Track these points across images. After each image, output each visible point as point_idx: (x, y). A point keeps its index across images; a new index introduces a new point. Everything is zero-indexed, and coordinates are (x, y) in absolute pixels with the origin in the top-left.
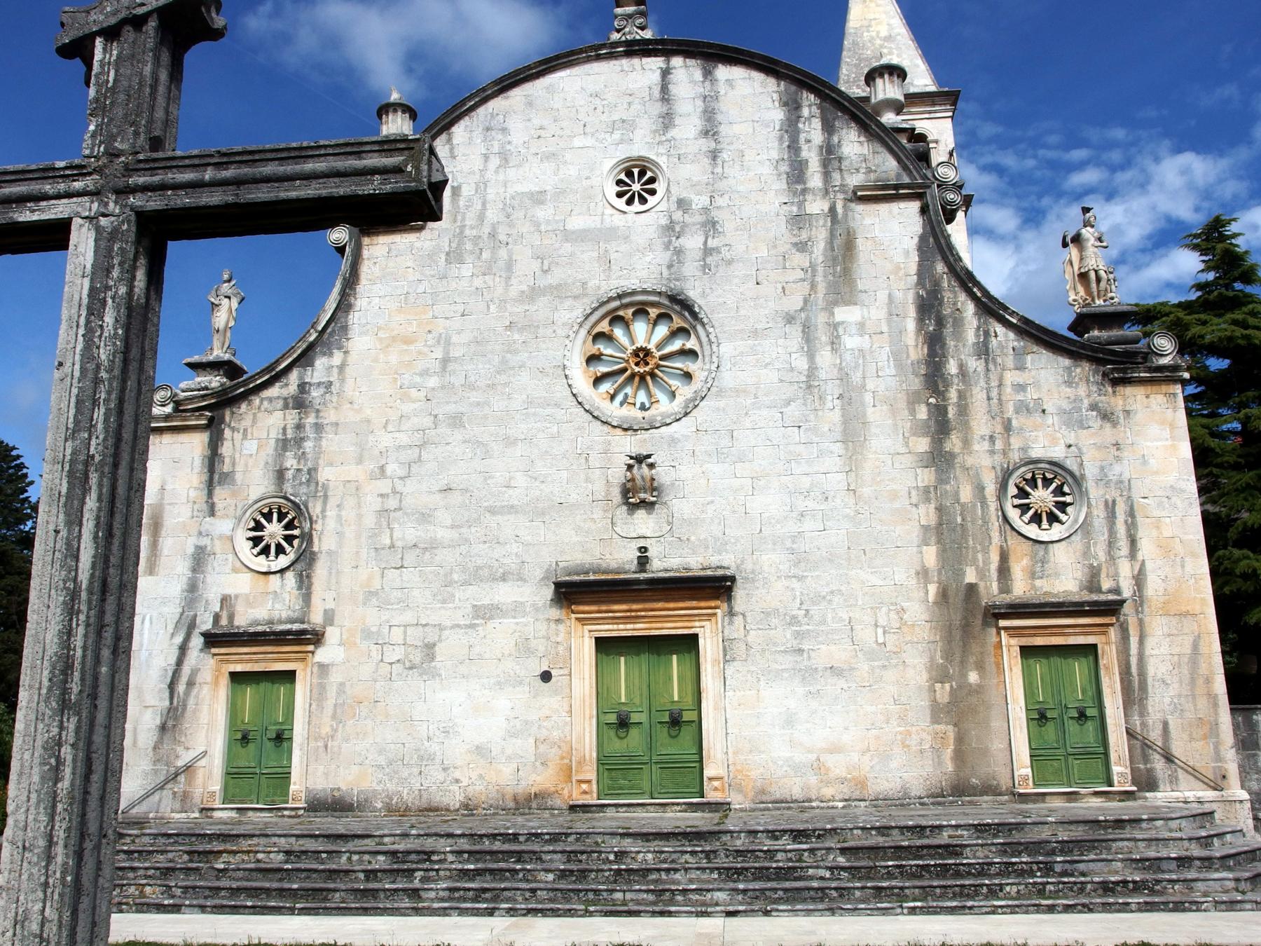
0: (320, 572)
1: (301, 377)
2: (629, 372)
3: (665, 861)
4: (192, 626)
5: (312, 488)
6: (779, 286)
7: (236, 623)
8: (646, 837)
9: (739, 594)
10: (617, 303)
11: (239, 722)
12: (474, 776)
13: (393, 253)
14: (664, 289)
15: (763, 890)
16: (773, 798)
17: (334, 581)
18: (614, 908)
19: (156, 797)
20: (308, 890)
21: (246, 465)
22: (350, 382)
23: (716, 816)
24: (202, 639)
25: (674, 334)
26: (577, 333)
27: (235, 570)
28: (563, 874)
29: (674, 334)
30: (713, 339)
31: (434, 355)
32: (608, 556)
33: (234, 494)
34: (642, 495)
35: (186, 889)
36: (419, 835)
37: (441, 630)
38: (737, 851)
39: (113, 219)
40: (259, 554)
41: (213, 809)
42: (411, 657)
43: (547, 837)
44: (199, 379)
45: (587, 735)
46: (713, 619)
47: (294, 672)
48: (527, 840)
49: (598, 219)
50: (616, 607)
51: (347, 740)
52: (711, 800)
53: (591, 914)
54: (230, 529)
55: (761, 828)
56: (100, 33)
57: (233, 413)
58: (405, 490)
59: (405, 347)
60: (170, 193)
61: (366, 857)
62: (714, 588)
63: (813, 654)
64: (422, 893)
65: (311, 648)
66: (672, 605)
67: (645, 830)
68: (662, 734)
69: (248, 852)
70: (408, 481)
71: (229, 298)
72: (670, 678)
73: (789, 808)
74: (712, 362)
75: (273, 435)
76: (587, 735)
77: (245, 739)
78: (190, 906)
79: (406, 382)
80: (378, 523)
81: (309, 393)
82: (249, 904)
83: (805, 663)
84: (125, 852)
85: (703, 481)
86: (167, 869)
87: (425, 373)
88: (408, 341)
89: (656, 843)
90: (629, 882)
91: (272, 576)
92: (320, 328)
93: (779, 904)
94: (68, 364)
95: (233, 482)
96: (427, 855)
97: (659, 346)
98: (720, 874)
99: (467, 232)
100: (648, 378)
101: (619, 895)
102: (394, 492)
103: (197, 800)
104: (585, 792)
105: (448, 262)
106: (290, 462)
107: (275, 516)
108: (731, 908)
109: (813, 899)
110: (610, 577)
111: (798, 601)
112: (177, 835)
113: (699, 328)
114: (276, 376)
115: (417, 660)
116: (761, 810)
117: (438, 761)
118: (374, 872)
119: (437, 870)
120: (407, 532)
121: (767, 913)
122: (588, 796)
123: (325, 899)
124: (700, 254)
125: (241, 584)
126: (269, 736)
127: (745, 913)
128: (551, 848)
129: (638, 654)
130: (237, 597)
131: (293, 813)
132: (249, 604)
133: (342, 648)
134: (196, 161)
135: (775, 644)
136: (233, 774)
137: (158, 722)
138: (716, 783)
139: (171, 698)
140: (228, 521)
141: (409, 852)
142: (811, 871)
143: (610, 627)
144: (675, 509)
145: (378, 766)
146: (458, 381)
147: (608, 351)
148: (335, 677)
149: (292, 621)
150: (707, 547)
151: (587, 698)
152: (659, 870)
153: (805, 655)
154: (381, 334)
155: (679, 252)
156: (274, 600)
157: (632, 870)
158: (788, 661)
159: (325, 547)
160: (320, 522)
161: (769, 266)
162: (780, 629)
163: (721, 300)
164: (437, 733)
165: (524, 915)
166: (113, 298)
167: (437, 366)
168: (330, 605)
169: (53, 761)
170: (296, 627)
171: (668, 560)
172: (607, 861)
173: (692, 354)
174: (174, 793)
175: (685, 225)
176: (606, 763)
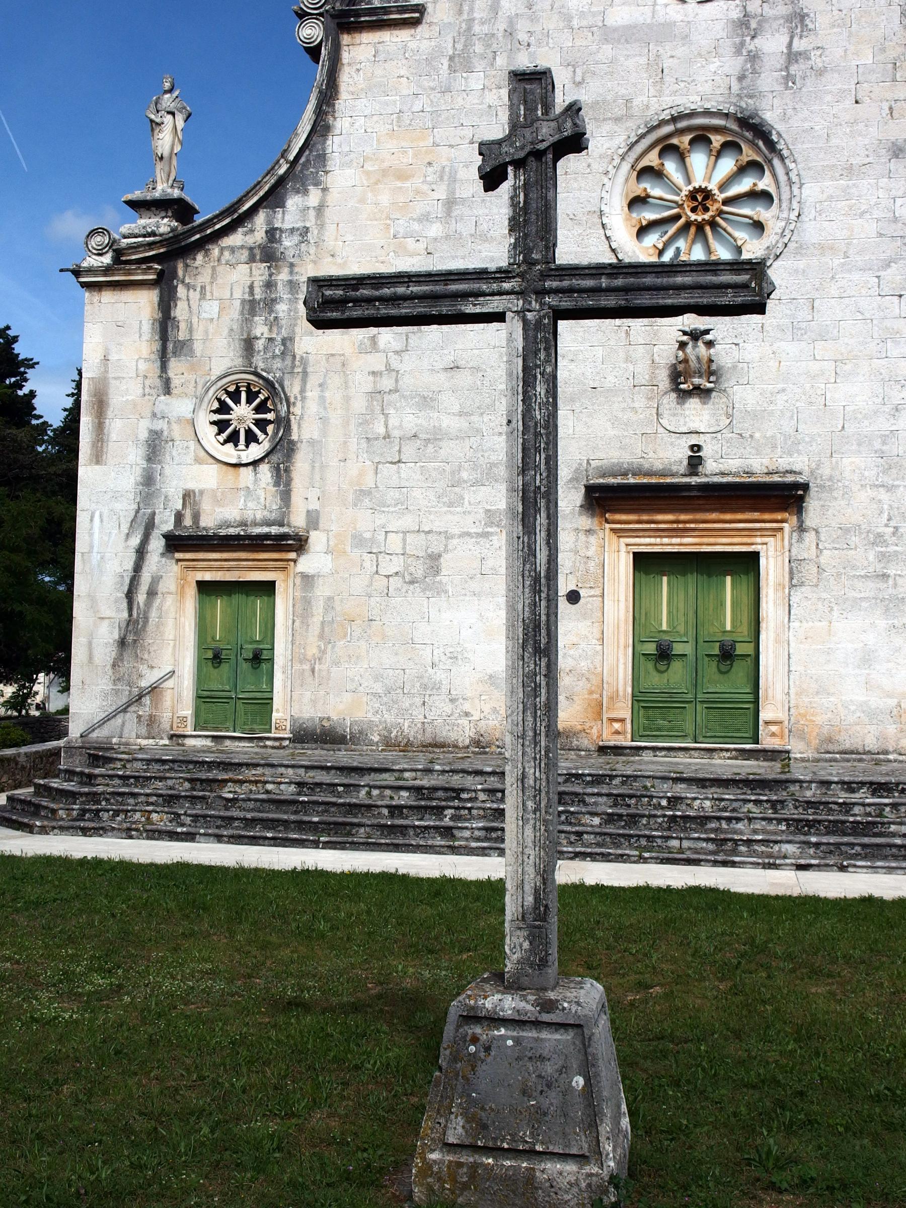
0: (301, 465)
1: (269, 222)
2: (682, 221)
3: (725, 809)
4: (150, 526)
5: (288, 361)
6: (886, 106)
7: (203, 524)
8: (702, 783)
9: (812, 505)
10: (669, 129)
11: (209, 639)
12: (487, 708)
13: (381, 57)
14: (732, 110)
15: (838, 845)
16: (841, 748)
17: (317, 477)
18: (671, 856)
19: (119, 720)
20: (330, 823)
21: (206, 332)
22: (330, 229)
23: (778, 766)
24: (163, 542)
25: (741, 170)
26: (617, 168)
27: (198, 461)
28: (610, 819)
29: (741, 170)
30: (794, 178)
31: (436, 195)
32: (651, 454)
33: (193, 368)
34: (696, 381)
35: (196, 817)
36: (444, 772)
37: (447, 538)
38: (808, 802)
39: (535, 313)
40: (226, 442)
41: (185, 736)
42: (412, 569)
43: (589, 778)
44: (142, 222)
45: (621, 667)
46: (779, 535)
47: (273, 583)
48: (566, 781)
49: (648, 10)
50: (660, 517)
51: (337, 663)
52: (767, 747)
53: (645, 861)
54: (188, 408)
55: (836, 779)
56: (510, 163)
57: (187, 266)
58: (402, 368)
59: (399, 184)
60: (576, 295)
61: (388, 792)
62: (782, 497)
63: (900, 581)
64: (455, 832)
65: (293, 555)
66: (728, 516)
67: (700, 776)
68: (710, 669)
69: (256, 782)
70: (406, 356)
71: (173, 114)
72: (722, 604)
73: (860, 760)
74: (791, 209)
75: (238, 294)
76: (621, 667)
77: (217, 658)
78: (205, 835)
79: (402, 231)
80: (371, 408)
81: (280, 241)
82: (269, 835)
83: (890, 591)
84: (120, 777)
85: (773, 364)
86: (171, 796)
87: (425, 218)
88: (402, 176)
89: (713, 790)
90: (685, 830)
91: (242, 469)
92: (291, 157)
93: (855, 859)
94: (514, 422)
95: (191, 353)
96: (457, 792)
97: (722, 187)
98: (788, 826)
99: (477, 28)
100: (708, 229)
101: (675, 843)
102: (389, 369)
103: (166, 725)
104: (617, 732)
105: (452, 69)
106: (260, 329)
107: (244, 396)
108: (802, 862)
109: (895, 857)
110: (654, 480)
111: (885, 516)
112: (173, 761)
113: (776, 162)
114: (236, 219)
115: (419, 574)
116: (826, 761)
117: (444, 690)
118: (400, 808)
119: (470, 809)
120: (405, 418)
121: (842, 869)
122: (621, 737)
123: (349, 834)
124: (782, 61)
125: (206, 478)
126: (245, 655)
127: (818, 867)
128: (596, 791)
129: (684, 574)
130: (202, 492)
131: (277, 744)
132: (217, 502)
133: (329, 557)
134: (594, 272)
135: (854, 568)
136: (205, 698)
137: (116, 636)
138: (774, 728)
139: (130, 609)
140: (187, 401)
141: (435, 789)
142: (893, 828)
143: (652, 540)
144: (737, 398)
145: (375, 694)
146: (466, 228)
147: (656, 191)
148: (322, 591)
149: (269, 524)
150: (774, 447)
151: (622, 625)
152: (719, 819)
153: (891, 582)
154: (369, 167)
155: (754, 57)
156: (246, 497)
157: (688, 817)
158: (869, 588)
159: (306, 436)
160: (299, 404)
161: (873, 77)
162: (861, 550)
163: (807, 125)
164: (443, 658)
165: (571, 859)
166: (542, 374)
167: (440, 210)
168: (314, 505)
169: (533, 685)
170: (274, 530)
171: (724, 463)
172: (659, 806)
173: (764, 197)
174: (139, 717)
175: (763, 19)
176: (641, 700)
